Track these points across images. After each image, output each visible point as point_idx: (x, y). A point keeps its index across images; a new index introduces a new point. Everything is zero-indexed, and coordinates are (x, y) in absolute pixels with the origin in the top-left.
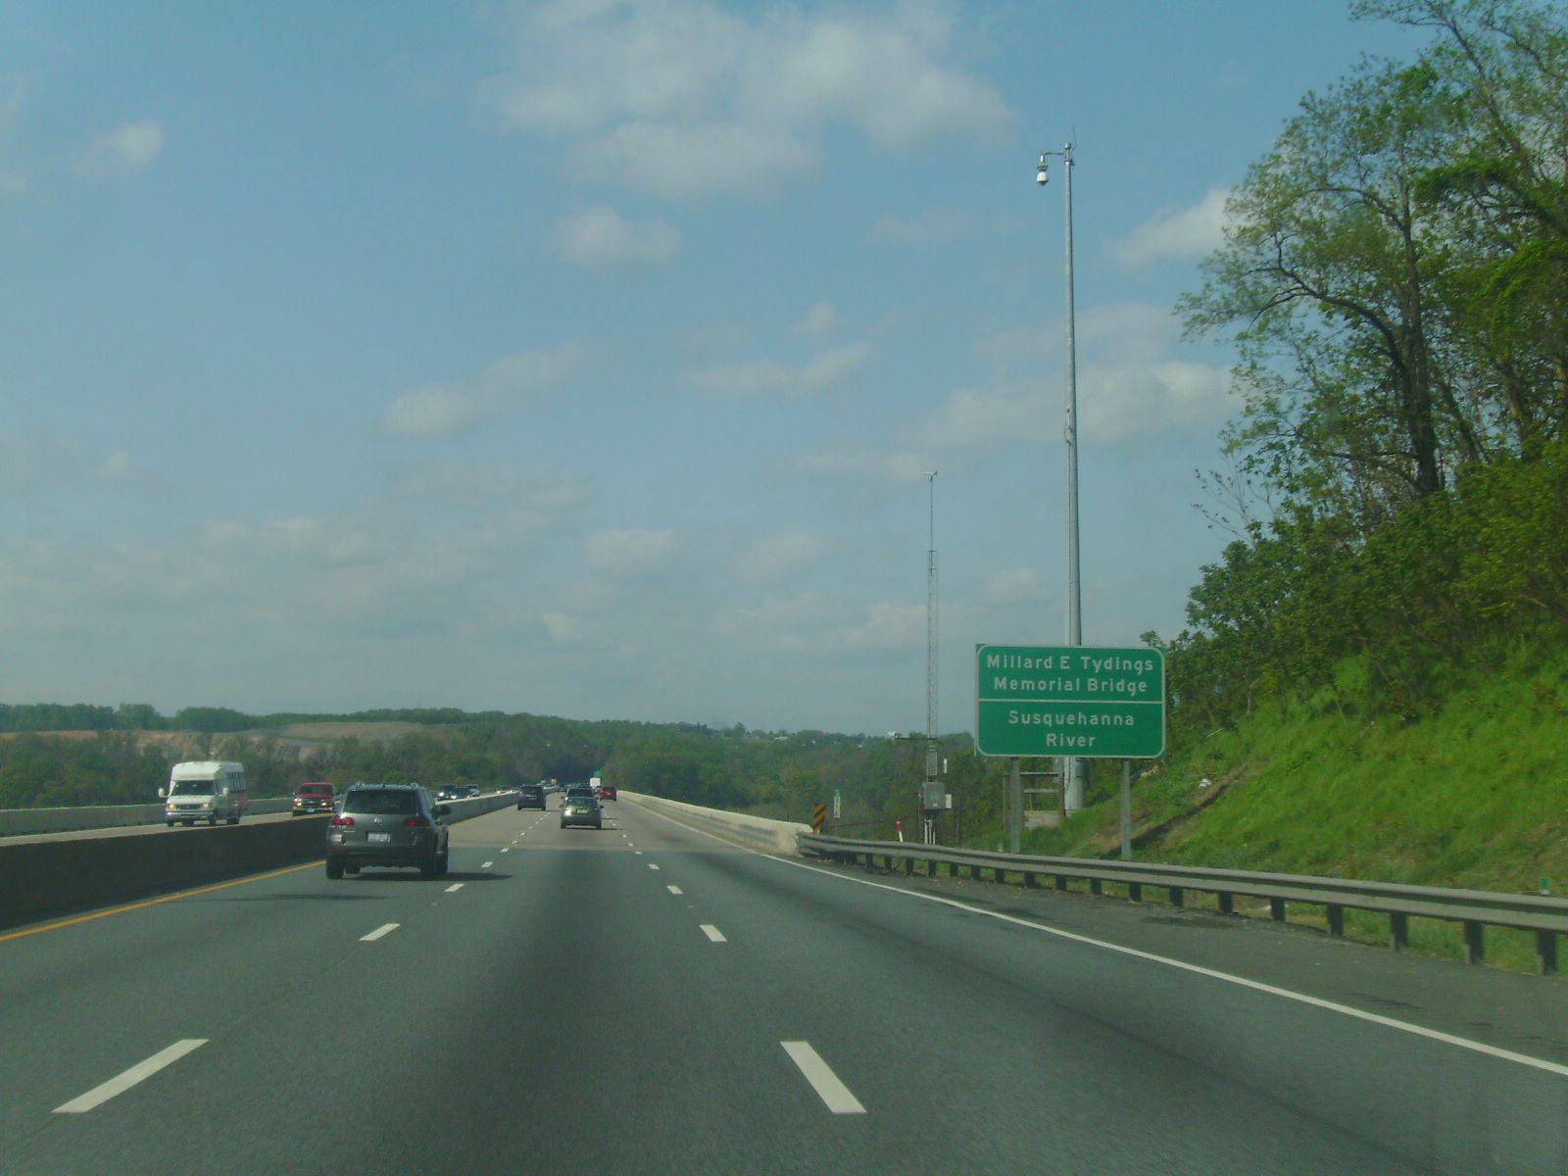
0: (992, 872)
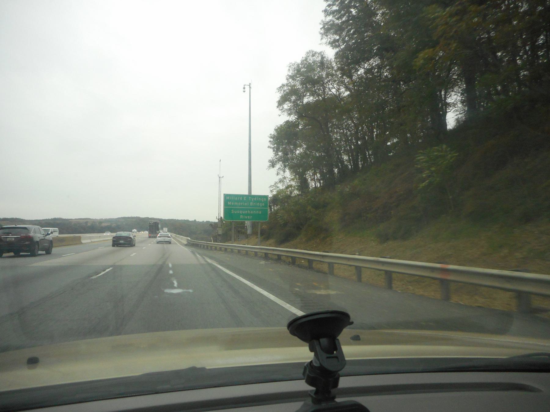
0: (219, 248)
